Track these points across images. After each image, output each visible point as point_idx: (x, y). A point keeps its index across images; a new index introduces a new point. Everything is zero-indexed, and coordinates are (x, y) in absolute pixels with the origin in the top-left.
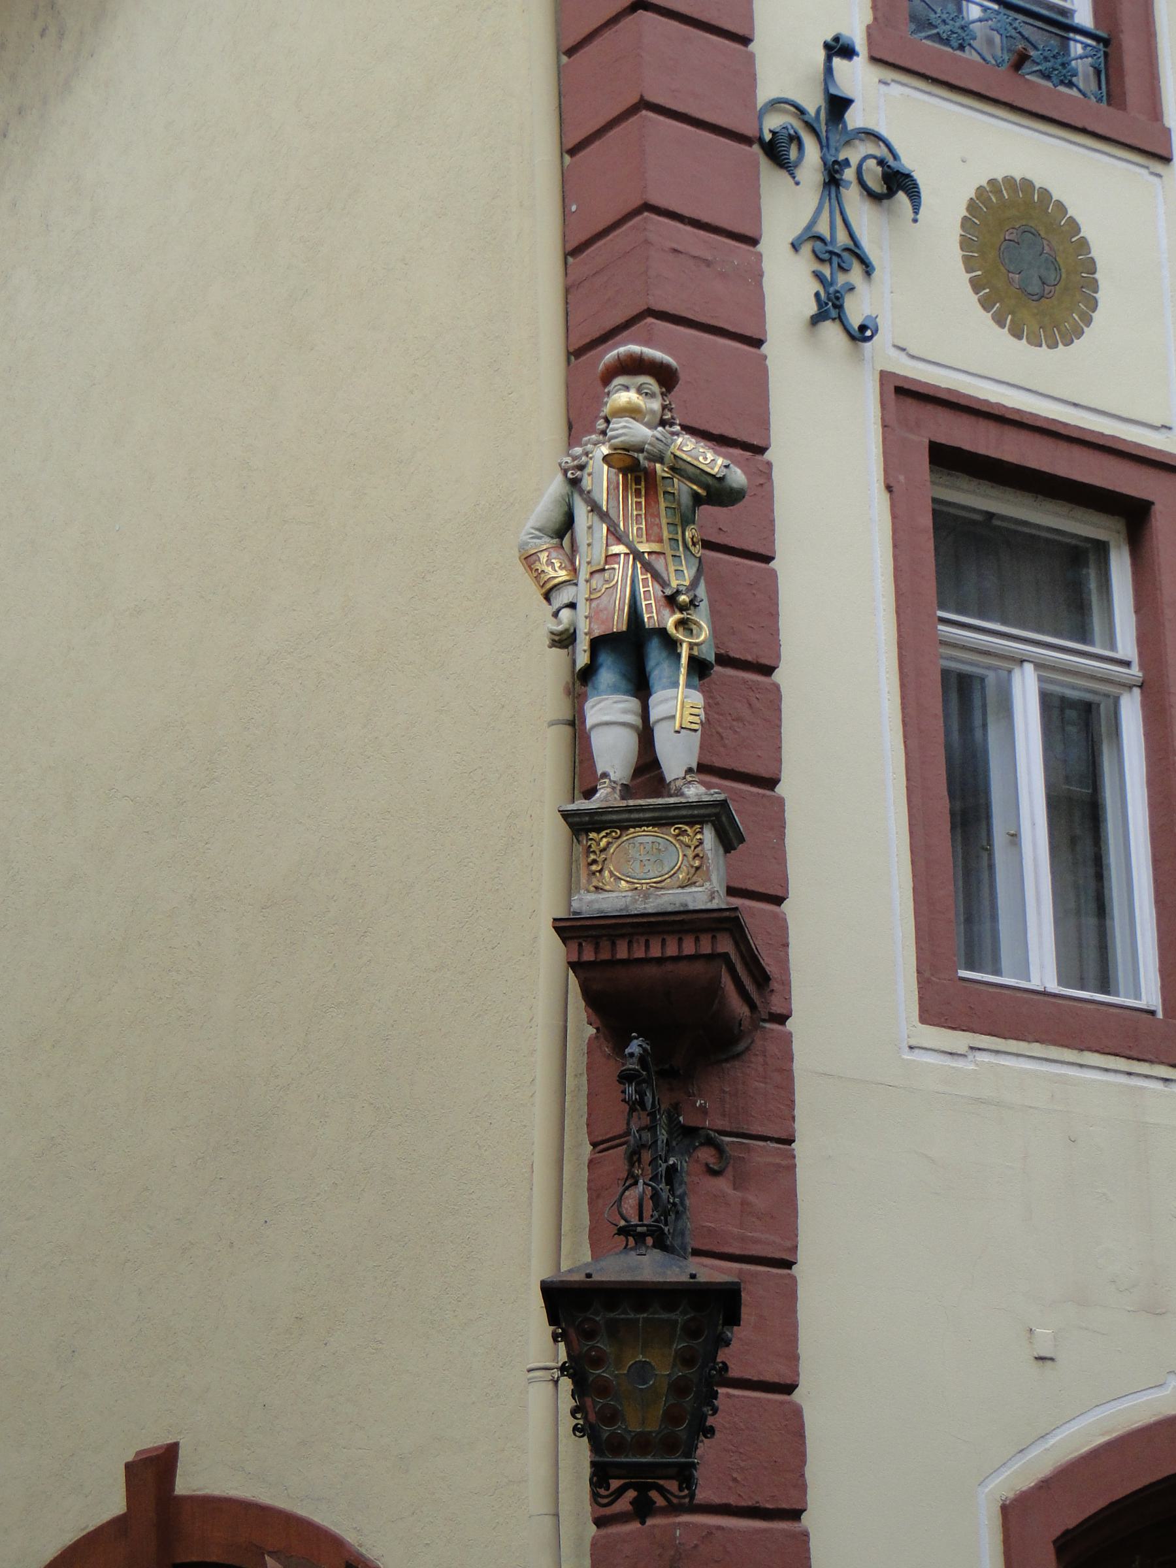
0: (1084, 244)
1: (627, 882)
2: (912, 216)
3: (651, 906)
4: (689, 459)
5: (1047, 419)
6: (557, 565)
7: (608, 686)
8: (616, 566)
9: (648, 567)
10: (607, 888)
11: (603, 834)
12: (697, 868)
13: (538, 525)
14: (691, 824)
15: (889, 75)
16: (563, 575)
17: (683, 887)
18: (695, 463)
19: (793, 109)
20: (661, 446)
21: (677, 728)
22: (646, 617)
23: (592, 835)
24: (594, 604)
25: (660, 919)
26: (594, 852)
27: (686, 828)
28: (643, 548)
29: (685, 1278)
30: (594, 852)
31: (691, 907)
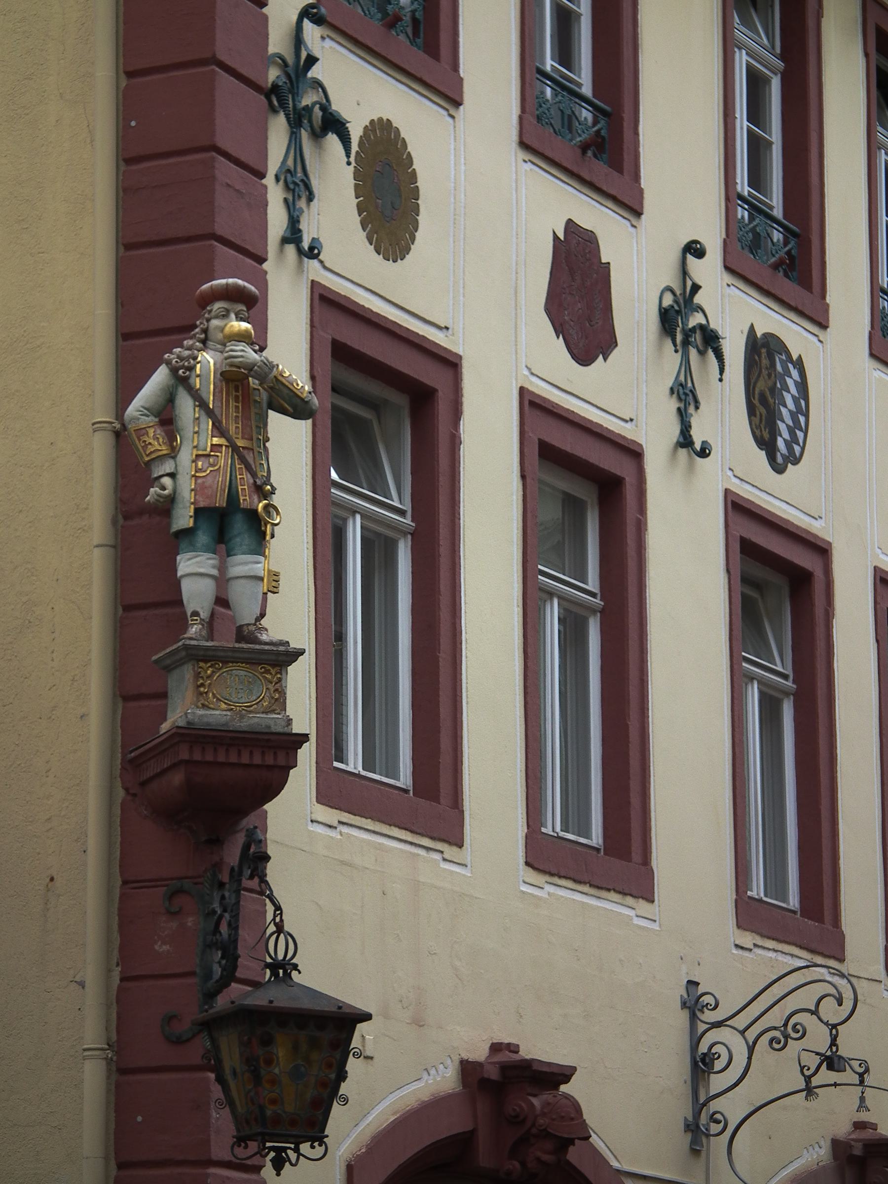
0: (414, 175)
1: (225, 703)
2: (346, 160)
3: (244, 725)
4: (287, 384)
5: (798, 527)
6: (161, 440)
7: (203, 545)
8: (218, 454)
9: (243, 460)
10: (212, 706)
11: (209, 664)
12: (276, 700)
13: (147, 406)
14: (274, 666)
15: (528, 157)
16: (165, 449)
17: (266, 713)
18: (291, 387)
19: (280, 61)
20: (267, 370)
21: (265, 591)
22: (242, 498)
23: (201, 664)
24: (199, 481)
25: (253, 736)
26: (202, 677)
27: (269, 668)
28: (240, 443)
29: (264, 1003)
30: (202, 677)
31: (273, 730)
